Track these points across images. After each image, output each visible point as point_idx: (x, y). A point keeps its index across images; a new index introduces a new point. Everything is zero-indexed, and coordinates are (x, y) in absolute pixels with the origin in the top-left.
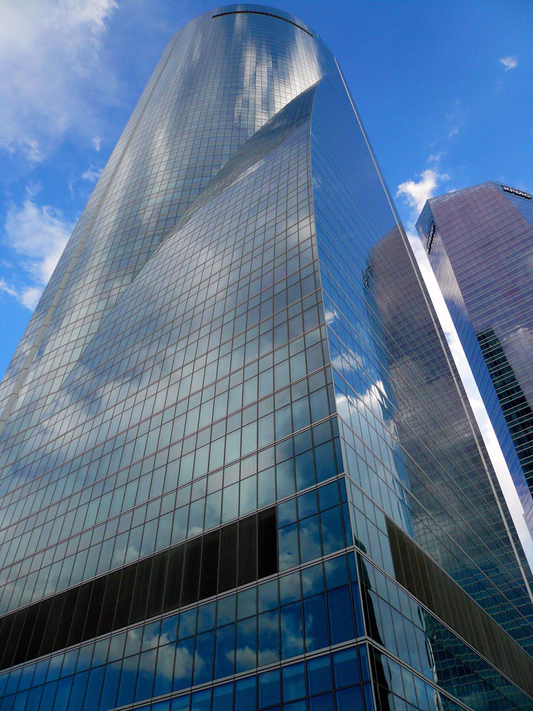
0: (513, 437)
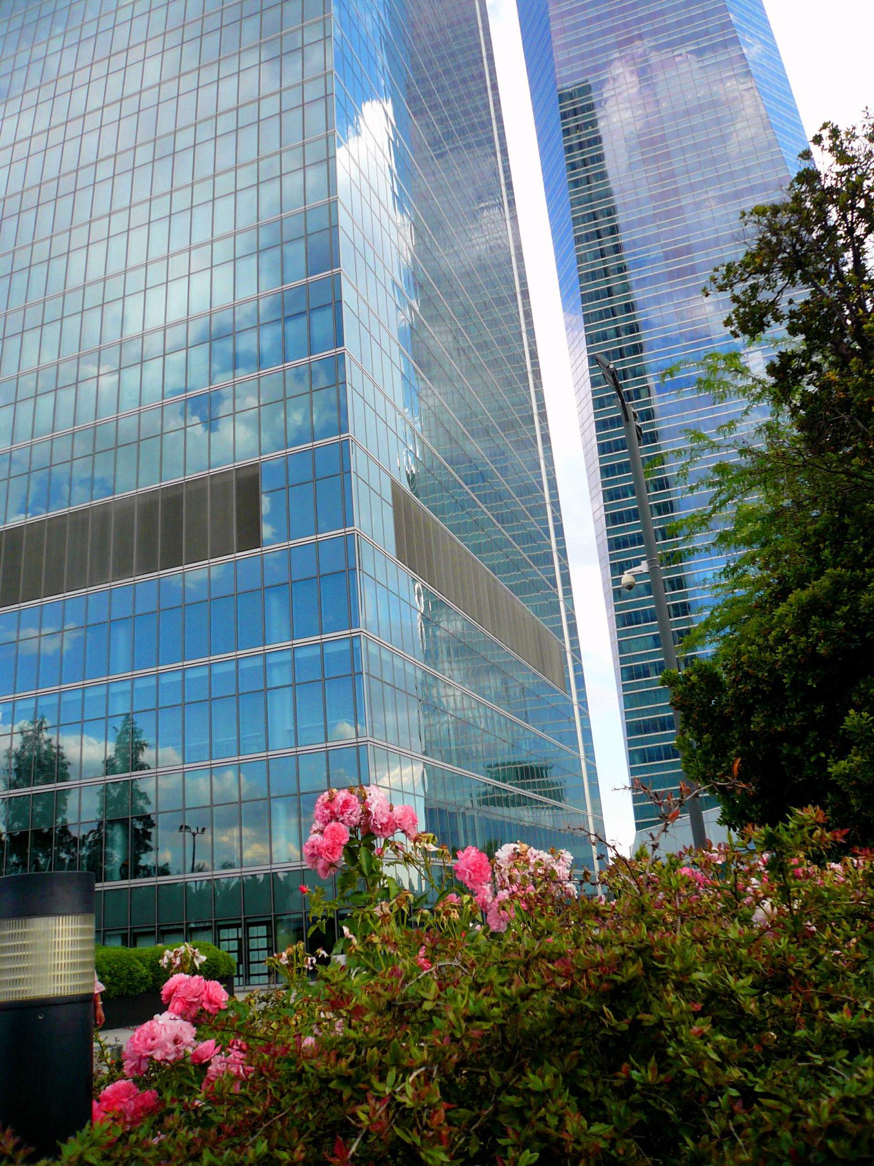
0: (571, 194)
